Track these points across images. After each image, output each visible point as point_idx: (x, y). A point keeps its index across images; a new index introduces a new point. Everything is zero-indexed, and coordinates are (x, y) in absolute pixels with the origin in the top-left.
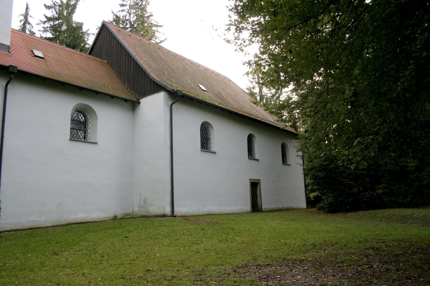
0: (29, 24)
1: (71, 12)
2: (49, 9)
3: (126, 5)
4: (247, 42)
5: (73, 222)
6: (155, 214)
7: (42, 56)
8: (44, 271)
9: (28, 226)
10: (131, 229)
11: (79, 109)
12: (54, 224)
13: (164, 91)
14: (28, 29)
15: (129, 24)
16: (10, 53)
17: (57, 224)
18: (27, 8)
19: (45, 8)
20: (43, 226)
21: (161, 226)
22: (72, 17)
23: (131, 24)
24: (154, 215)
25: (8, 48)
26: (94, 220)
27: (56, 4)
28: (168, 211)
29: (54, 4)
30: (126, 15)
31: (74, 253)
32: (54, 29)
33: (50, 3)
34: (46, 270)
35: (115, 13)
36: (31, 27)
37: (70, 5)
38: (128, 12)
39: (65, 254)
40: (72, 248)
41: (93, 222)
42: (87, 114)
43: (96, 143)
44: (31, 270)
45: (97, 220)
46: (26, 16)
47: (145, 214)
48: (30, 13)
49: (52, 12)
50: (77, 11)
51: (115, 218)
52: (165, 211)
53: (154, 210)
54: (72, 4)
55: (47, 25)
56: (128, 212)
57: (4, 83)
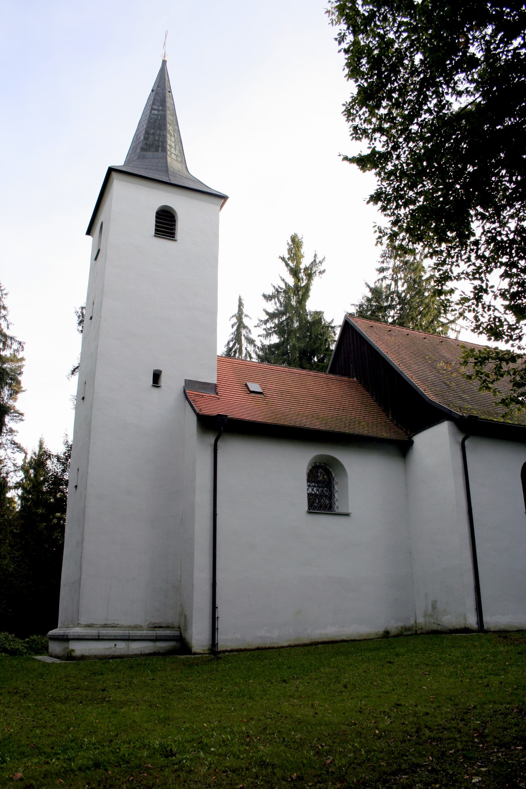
0: (245, 327)
1: (302, 300)
2: (271, 300)
3: (387, 269)
4: (493, 377)
5: (320, 641)
6: (452, 628)
7: (259, 390)
8: (265, 700)
9: (255, 645)
10: (402, 650)
11: (318, 464)
12: (292, 643)
13: (447, 420)
14: (244, 336)
15: (397, 299)
16: (217, 394)
17: (296, 643)
18: (241, 305)
19: (265, 301)
20: (275, 646)
21: (453, 647)
22: (305, 306)
23: (399, 297)
24: (450, 630)
25: (214, 388)
26: (353, 638)
27: (280, 290)
28: (472, 621)
29: (277, 290)
30: (391, 284)
31: (309, 681)
32: (280, 330)
33: (270, 291)
34: (267, 699)
35: (372, 286)
36: (248, 331)
37: (301, 287)
38: (392, 279)
39: (297, 682)
40: (308, 675)
41: (352, 640)
42: (331, 470)
43: (347, 515)
44: (251, 698)
45: (357, 638)
46: (240, 316)
47: (435, 627)
48: (245, 311)
49: (276, 303)
50: (311, 293)
51: (387, 634)
52: (468, 623)
53: (450, 620)
54: (302, 285)
55: (270, 325)
56: (408, 625)
57: (212, 441)
